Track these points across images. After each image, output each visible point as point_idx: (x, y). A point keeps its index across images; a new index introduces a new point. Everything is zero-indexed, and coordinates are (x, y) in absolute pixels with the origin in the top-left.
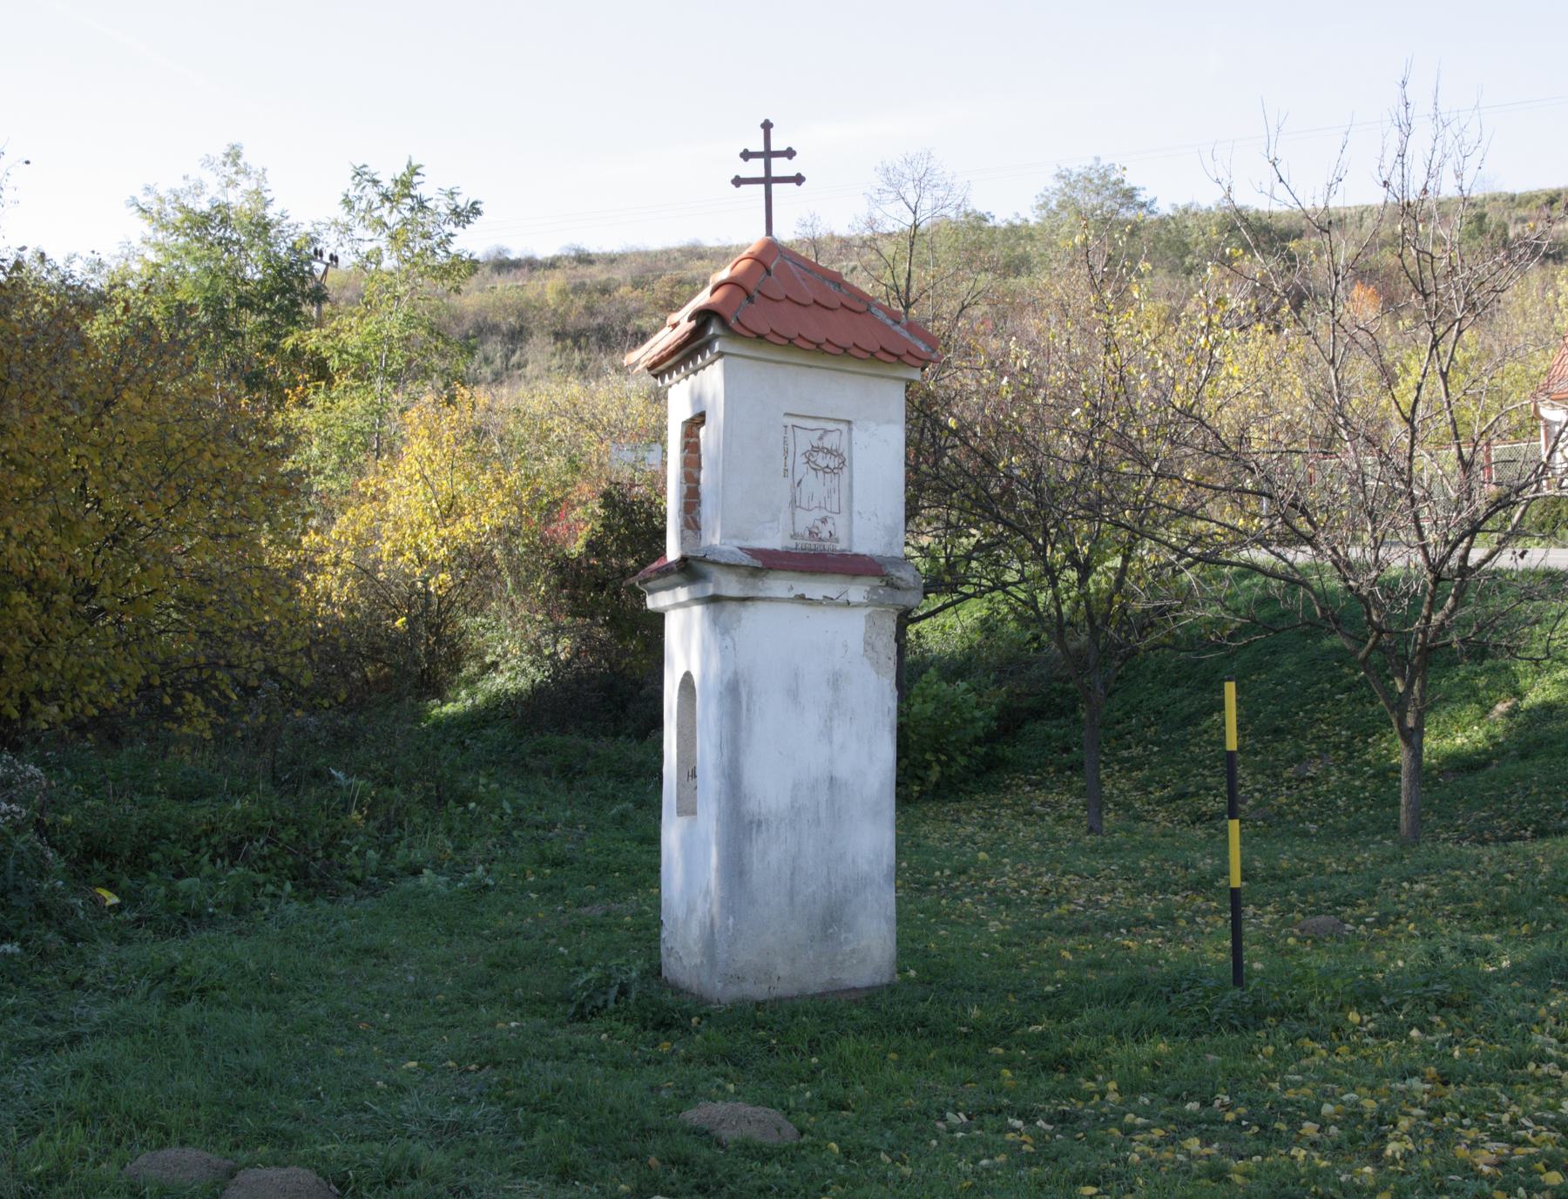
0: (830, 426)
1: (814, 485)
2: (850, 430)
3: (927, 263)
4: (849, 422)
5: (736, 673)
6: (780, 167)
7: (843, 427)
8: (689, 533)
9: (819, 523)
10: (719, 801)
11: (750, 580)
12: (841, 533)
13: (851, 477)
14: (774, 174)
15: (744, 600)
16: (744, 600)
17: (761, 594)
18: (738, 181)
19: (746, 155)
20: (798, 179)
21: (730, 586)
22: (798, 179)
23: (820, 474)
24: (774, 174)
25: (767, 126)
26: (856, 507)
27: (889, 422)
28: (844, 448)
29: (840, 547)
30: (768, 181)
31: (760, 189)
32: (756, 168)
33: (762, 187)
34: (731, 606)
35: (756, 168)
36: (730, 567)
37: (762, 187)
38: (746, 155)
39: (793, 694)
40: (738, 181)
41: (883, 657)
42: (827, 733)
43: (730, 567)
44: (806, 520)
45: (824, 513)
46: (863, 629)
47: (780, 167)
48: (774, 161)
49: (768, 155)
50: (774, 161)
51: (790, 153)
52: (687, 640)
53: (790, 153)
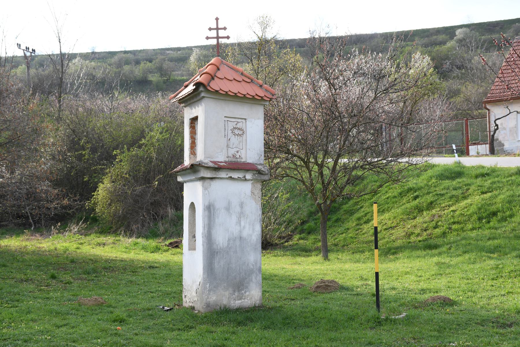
0: (239, 120)
1: (234, 140)
2: (246, 122)
4: (245, 119)
7: (244, 121)
8: (192, 156)
10: (203, 245)
11: (214, 172)
12: (243, 156)
15: (212, 179)
16: (212, 179)
17: (218, 176)
19: (210, 29)
23: (236, 136)
25: (217, 19)
26: (248, 147)
36: (208, 168)
38: (210, 29)
39: (228, 209)
41: (257, 197)
43: (208, 168)
44: (231, 152)
49: (217, 29)
51: (225, 29)
52: (193, 193)
53: (225, 29)
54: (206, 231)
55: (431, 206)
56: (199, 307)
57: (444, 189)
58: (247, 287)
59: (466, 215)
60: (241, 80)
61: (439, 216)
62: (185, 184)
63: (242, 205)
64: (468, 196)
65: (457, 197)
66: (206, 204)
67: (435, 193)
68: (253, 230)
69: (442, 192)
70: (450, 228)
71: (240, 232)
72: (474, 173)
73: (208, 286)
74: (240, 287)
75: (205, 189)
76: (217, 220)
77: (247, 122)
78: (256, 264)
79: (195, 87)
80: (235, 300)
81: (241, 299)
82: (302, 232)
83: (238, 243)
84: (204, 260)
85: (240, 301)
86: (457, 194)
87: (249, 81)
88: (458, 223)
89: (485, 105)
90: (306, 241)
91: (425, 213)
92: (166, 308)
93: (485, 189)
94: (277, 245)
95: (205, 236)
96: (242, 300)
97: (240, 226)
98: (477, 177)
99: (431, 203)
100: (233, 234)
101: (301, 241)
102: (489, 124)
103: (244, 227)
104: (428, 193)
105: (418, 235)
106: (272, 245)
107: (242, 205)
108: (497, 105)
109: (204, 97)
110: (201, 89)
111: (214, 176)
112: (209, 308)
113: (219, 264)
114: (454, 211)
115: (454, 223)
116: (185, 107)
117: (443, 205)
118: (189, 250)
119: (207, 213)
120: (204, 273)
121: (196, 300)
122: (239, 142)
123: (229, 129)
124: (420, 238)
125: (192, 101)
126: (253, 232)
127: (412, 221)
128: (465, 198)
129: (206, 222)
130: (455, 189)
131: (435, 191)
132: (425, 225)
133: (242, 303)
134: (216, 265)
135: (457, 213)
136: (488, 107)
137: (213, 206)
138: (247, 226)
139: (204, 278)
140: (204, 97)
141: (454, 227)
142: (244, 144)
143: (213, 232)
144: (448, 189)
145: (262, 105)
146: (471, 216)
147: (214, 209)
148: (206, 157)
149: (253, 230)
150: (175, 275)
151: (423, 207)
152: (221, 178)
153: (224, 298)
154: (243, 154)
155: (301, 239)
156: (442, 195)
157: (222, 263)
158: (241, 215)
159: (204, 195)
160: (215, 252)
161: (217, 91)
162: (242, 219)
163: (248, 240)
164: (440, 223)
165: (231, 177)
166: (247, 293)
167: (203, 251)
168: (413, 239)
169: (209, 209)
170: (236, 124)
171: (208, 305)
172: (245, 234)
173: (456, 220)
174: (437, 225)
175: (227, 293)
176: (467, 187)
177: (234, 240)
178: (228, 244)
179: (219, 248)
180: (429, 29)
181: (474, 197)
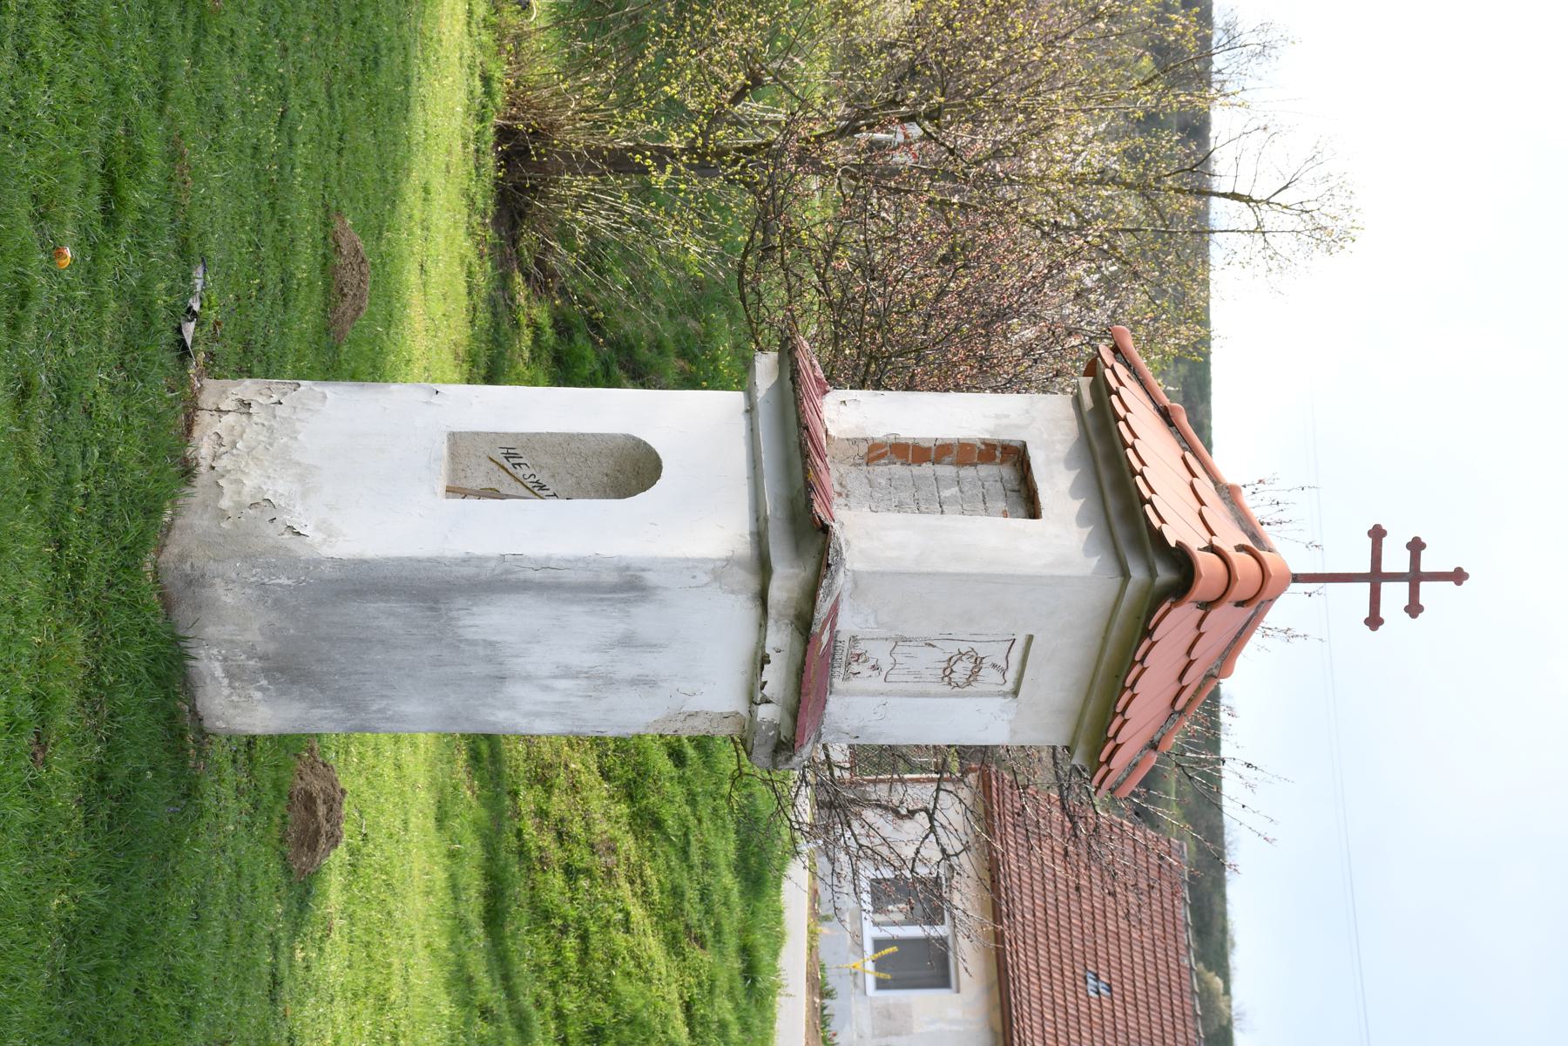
0: (1011, 675)
1: (931, 660)
2: (1005, 695)
3: (1129, 254)
4: (1015, 693)
5: (656, 588)
6: (1394, 595)
7: (1009, 686)
8: (864, 448)
9: (872, 662)
10: (466, 561)
11: (792, 612)
12: (855, 683)
13: (936, 696)
14: (1386, 587)
15: (762, 597)
16: (762, 597)
17: (771, 622)
18: (1377, 534)
19: (1416, 546)
20: (1374, 621)
21: (785, 583)
22: (1374, 621)
23: (945, 665)
24: (1386, 587)
25: (1458, 576)
26: (892, 701)
27: (1013, 732)
28: (976, 687)
29: (838, 682)
30: (1376, 577)
31: (1366, 568)
32: (1395, 559)
33: (1367, 569)
34: (753, 584)
35: (1395, 559)
36: (811, 595)
37: (1367, 569)
38: (1416, 546)
39: (627, 642)
40: (1377, 534)
41: (679, 725)
42: (568, 673)
43: (811, 595)
44: (879, 652)
45: (886, 668)
46: (714, 556)
47: (1394, 595)
48: (1404, 587)
49: (1415, 577)
50: (1404, 587)
51: (1414, 609)
52: (699, 430)
53: (1414, 609)
54: (530, 574)
55: (647, 823)
56: (193, 526)
57: (705, 849)
58: (282, 693)
59: (609, 976)
60: (1184, 683)
61: (609, 873)
62: (741, 394)
63: (644, 682)
64: (681, 954)
65: (677, 912)
66: (646, 575)
67: (692, 821)
68: (538, 715)
69: (694, 850)
70: (564, 931)
71: (528, 678)
72: (758, 937)
73: (284, 581)
74: (285, 671)
75: (719, 571)
76: (576, 609)
77: (1001, 700)
78: (390, 719)
79: (1173, 544)
80: (225, 659)
81: (230, 675)
82: (563, 327)
83: (478, 669)
84: (401, 562)
85: (219, 673)
86: (687, 906)
87: (1178, 706)
88: (584, 953)
89: (974, 770)
90: (527, 355)
91: (623, 808)
92: (189, 329)
93: (700, 1010)
94: (515, 242)
95: (508, 572)
96: (226, 682)
97: (555, 677)
98: (746, 951)
99: (658, 824)
100: (517, 656)
101: (527, 336)
102: (918, 781)
103: (547, 688)
104: (692, 800)
105: (542, 814)
106: (514, 226)
107: (644, 682)
108: (989, 988)
109: (1125, 574)
110: (1164, 575)
111: (772, 612)
112: (180, 584)
113: (383, 616)
114: (626, 926)
115: (584, 938)
116: (1077, 400)
117: (649, 872)
118: (455, 439)
119: (610, 578)
120: (340, 563)
121: (225, 503)
122: (918, 675)
123: (973, 645)
124: (529, 826)
125: (1098, 448)
126: (531, 710)
127: (594, 768)
128: (673, 945)
129: (569, 576)
130: (704, 895)
131: (700, 821)
132: (577, 828)
133: (214, 678)
134: (374, 607)
135: (619, 937)
136: (972, 778)
137: (643, 599)
138: (555, 697)
139: (318, 563)
140: (1125, 574)
141: (571, 942)
142: (911, 687)
143: (526, 599)
144: (707, 866)
145: (1074, 740)
146: (608, 994)
147: (626, 601)
148: (856, 578)
149: (538, 715)
150: (345, 344)
151: (644, 796)
152: (762, 625)
153: (230, 628)
154: (866, 680)
155: (537, 329)
156: (685, 853)
157: (388, 624)
158: (604, 682)
159: (690, 566)
160: (437, 602)
161: (1148, 633)
162: (584, 683)
163: (490, 700)
164: (584, 883)
165: (765, 660)
166: (258, 695)
167: (435, 562)
168: (528, 799)
169: (628, 586)
170: (994, 666)
171: (193, 582)
172: (515, 690)
173: (595, 940)
174: (579, 871)
175: (253, 635)
176: (709, 933)
177: (489, 660)
178: (473, 643)
179: (455, 614)
180: (1209, 402)
181: (675, 974)
